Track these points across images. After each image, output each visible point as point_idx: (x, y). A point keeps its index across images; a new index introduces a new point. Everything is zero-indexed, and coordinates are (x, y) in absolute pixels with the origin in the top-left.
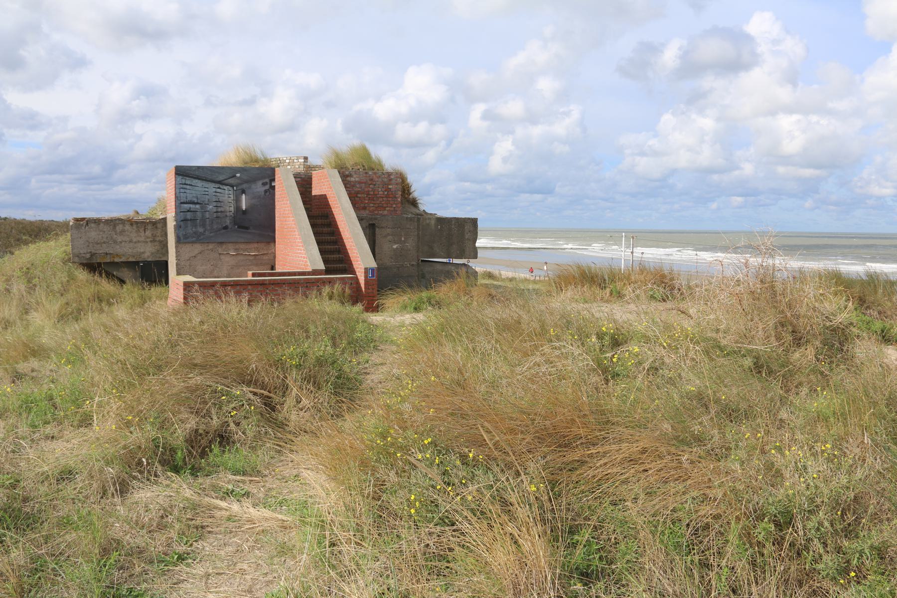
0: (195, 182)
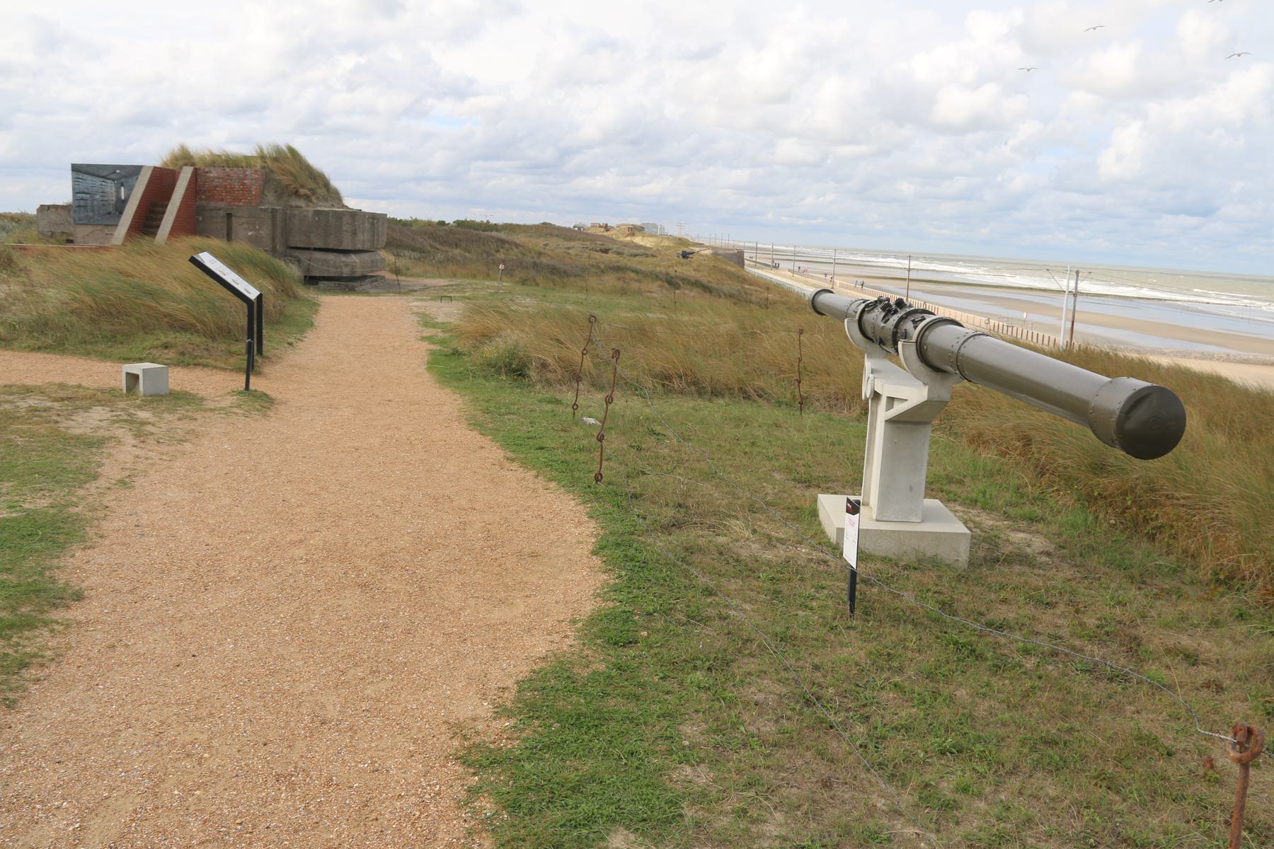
0: (86, 176)
